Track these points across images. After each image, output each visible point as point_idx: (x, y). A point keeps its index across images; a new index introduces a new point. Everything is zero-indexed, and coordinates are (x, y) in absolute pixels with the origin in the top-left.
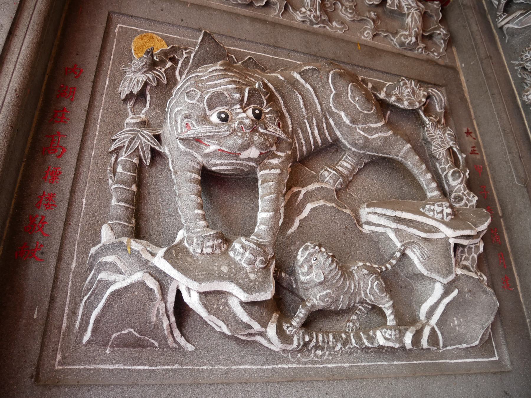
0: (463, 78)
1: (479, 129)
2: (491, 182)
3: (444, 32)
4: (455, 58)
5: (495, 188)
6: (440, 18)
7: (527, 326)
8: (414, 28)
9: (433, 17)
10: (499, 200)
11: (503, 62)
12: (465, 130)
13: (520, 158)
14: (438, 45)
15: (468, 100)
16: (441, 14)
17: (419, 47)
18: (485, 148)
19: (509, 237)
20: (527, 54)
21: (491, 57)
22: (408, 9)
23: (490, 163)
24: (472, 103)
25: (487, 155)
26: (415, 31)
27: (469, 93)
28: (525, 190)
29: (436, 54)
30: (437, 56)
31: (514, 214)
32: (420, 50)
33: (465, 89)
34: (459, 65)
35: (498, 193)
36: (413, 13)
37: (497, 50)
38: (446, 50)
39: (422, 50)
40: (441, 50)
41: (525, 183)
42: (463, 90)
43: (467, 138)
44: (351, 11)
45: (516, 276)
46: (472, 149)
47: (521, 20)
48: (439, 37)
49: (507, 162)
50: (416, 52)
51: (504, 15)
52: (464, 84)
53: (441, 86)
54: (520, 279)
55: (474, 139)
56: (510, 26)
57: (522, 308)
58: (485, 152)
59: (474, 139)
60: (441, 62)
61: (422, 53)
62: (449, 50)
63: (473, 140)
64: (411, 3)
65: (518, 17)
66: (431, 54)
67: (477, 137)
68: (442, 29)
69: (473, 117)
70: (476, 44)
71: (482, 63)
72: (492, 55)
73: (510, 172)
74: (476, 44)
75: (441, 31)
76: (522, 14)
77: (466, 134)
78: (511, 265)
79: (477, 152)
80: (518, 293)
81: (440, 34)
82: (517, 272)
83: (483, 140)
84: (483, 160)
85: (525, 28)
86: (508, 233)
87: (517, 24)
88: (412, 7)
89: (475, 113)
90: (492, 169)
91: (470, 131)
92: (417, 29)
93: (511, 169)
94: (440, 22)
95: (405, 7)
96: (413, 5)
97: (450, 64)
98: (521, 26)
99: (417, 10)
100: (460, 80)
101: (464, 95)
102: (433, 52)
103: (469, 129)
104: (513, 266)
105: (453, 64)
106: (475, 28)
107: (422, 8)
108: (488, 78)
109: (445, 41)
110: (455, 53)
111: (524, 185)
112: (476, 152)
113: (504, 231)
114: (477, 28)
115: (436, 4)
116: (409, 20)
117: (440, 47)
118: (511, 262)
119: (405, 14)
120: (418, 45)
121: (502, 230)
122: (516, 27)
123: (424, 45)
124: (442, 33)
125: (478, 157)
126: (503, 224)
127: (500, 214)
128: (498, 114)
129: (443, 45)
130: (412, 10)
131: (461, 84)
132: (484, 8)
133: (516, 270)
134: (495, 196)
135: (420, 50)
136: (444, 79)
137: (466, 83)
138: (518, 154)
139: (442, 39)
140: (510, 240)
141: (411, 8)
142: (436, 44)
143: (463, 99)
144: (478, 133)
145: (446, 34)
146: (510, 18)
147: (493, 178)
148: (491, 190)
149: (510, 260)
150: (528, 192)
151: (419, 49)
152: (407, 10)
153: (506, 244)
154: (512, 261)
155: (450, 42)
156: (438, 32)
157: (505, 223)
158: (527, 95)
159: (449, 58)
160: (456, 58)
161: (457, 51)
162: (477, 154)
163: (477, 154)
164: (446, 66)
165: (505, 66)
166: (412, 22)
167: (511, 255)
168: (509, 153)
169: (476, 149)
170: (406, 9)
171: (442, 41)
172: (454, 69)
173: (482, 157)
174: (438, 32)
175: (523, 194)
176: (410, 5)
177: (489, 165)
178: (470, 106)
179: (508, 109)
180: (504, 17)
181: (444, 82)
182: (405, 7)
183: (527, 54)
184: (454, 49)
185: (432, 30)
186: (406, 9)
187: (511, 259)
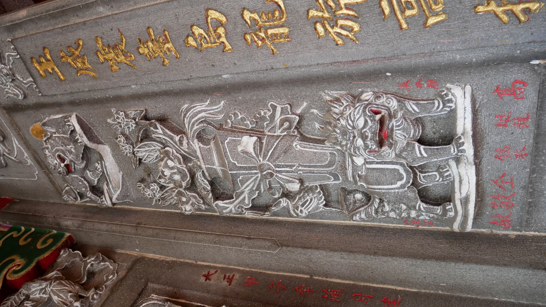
0: (151, 255)
1: (208, 262)
2: (269, 272)
3: (93, 259)
4: (127, 254)
5: (277, 271)
6: (81, 254)
7: (448, 296)
8: (67, 297)
9: (76, 260)
10: (291, 272)
11: (150, 211)
12: (203, 279)
13: (249, 238)
14: (105, 268)
15: (175, 259)
16: (76, 252)
17: (91, 297)
18: (231, 265)
19: (337, 278)
20: (147, 194)
21: (139, 223)
22: (45, 293)
23: (248, 266)
24: (179, 258)
25: (239, 266)
26: (71, 296)
27: (167, 256)
28: (284, 248)
29: (111, 277)
30: (114, 276)
31: (311, 266)
32: (95, 296)
33: (163, 257)
34: (136, 253)
35: (283, 271)
36: (52, 290)
37: (136, 212)
38: (115, 262)
39: (97, 294)
40: (111, 267)
41: (278, 245)
42: (163, 261)
43: (212, 282)
44: (229, 121)
45: (385, 286)
46: (226, 280)
47: (113, 187)
48: (95, 265)
49: (250, 252)
50: (95, 301)
51: (102, 198)
52: (157, 257)
53: (145, 287)
54: (388, 284)
55: (216, 272)
56: (115, 197)
57: (425, 293)
58: (234, 266)
59: (216, 272)
60: (122, 273)
61: (100, 294)
62: (116, 257)
63: (217, 274)
64: (41, 287)
65: (109, 189)
66: (108, 283)
67: (215, 268)
68: (88, 261)
69: (194, 262)
70: (120, 232)
71: (140, 235)
72: (138, 221)
73: (262, 253)
74: (120, 232)
75: (90, 262)
76: (108, 185)
77: (208, 281)
78: (370, 287)
79: (231, 275)
80: (405, 291)
81: (92, 265)
82: (379, 284)
83: (220, 263)
84: (243, 271)
85: (123, 185)
86: (331, 277)
87: (115, 191)
88: (45, 288)
89: (189, 259)
90: (255, 266)
91: (206, 273)
92: (69, 294)
93: (259, 252)
94: (84, 256)
95: (41, 295)
96: (44, 286)
97: (130, 263)
98: (119, 189)
99: (51, 284)
100: (151, 259)
101: (167, 262)
102: (108, 280)
103: (204, 273)
104: (371, 285)
105: (133, 259)
106: (104, 227)
107: (56, 274)
108: (157, 236)
109: (103, 261)
110: (123, 252)
111: (279, 247)
112: (231, 277)
113: (329, 280)
114: (105, 225)
115: (63, 254)
116: (55, 298)
117: (108, 266)
118: (367, 286)
119: (48, 298)
120: (88, 298)
121: (327, 281)
122: (119, 192)
123: (93, 289)
124: (92, 262)
125: (237, 276)
126: (320, 278)
127: (309, 277)
128: (196, 242)
129: (108, 263)
130: (49, 289)
131: (155, 260)
132: (94, 206)
133: (377, 284)
134: (286, 274)
135: (95, 296)
136: (141, 279)
137: (156, 254)
138: (244, 239)
139: (99, 263)
140: (339, 277)
141: (46, 290)
142: (102, 271)
143: (171, 265)
144: (212, 264)
145: (97, 257)
146: (107, 195)
147: (265, 269)
148: (277, 275)
149: (364, 286)
150: (288, 246)
151: (93, 299)
152: (46, 294)
153: (344, 284)
154: (365, 284)
155: (108, 253)
156: (89, 266)
157: (319, 276)
158: (186, 210)
159: (123, 261)
160: (128, 252)
161: (123, 248)
162: (234, 275)
163: (234, 275)
164: (130, 269)
165: (155, 211)
166: (59, 296)
167: (357, 283)
168: (241, 247)
169: (227, 275)
170: (44, 296)
171: (102, 263)
172: (139, 260)
173: (238, 271)
174: (89, 266)
175: (289, 251)
176: (42, 289)
177: (250, 268)
178: (182, 260)
179: (195, 229)
180: (104, 199)
181: (143, 280)
182: (41, 295)
183: (147, 194)
184: (119, 251)
185: (84, 271)
186: (44, 296)
187: (362, 284)
